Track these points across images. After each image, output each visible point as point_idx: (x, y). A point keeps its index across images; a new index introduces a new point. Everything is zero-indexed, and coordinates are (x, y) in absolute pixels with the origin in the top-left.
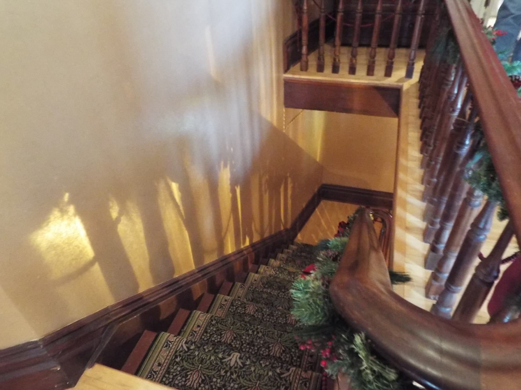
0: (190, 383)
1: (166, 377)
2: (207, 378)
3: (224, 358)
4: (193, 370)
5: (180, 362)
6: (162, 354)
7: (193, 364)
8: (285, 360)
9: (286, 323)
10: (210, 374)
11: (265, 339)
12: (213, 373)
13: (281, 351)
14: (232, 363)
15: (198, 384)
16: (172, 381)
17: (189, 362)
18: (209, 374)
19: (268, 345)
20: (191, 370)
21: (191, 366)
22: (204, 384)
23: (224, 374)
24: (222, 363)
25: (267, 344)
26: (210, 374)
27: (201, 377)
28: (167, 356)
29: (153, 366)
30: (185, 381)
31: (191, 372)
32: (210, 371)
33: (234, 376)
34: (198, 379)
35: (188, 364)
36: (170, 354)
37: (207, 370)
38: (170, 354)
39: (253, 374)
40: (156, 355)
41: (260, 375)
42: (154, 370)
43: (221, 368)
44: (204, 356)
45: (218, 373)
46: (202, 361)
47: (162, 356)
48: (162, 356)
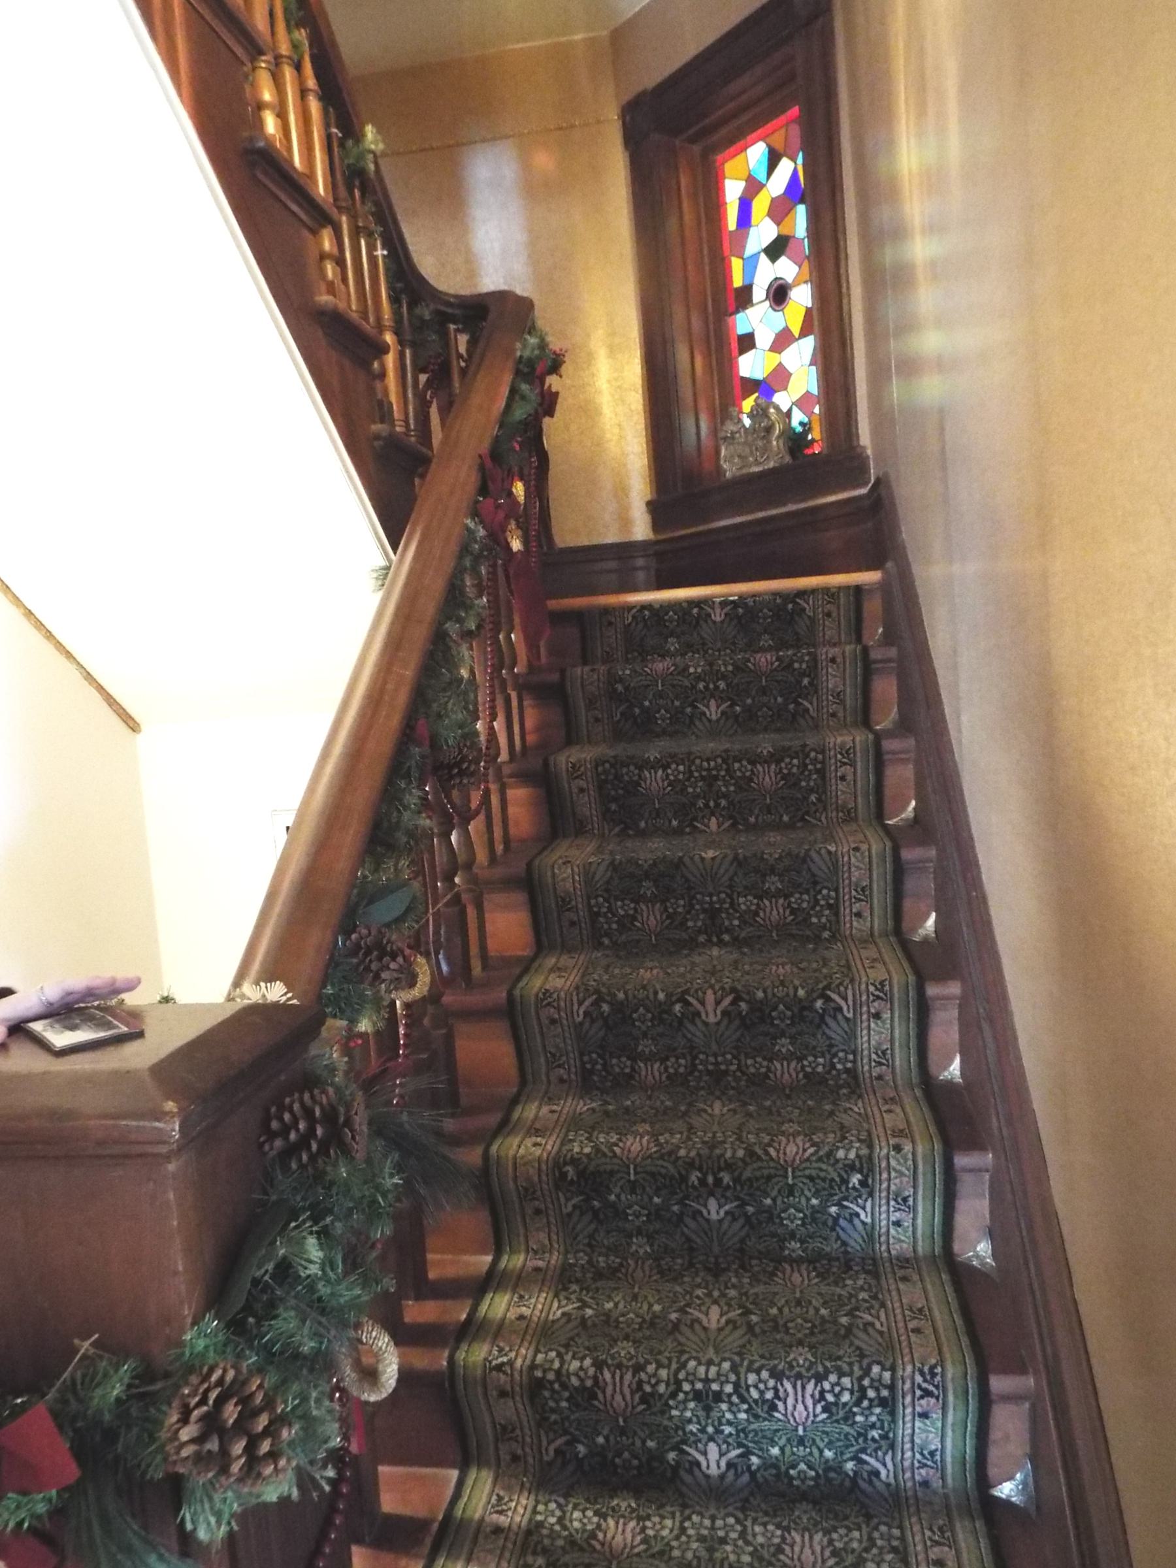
0: (779, 905)
1: (886, 1387)
2: (751, 921)
3: (731, 706)
4: (772, 671)
5: (849, 1176)
6: (905, 1179)
7: (811, 1178)
8: (583, 1511)
9: (663, 902)
10: (755, 1166)
11: (674, 1163)
12: (749, 1169)
13: (639, 917)
14: (713, 703)
15: (781, 1394)
16: (815, 896)
17: (824, 1180)
18: (760, 1164)
19: (649, 1407)
20: (808, 1160)
21: (814, 1173)
22: (765, 1401)
23: (722, 1174)
24: (730, 699)
25: (678, 789)
26: (755, 1166)
27: (778, 1151)
28: (889, 1180)
29: (855, 773)
30: (822, 1392)
31: (807, 1154)
32: (758, 1174)
33: (701, 685)
34: (790, 1408)
35: (822, 1174)
36: (885, 1185)
37: (766, 1172)
38: (885, 1185)
39: (669, 815)
40: (848, 671)
41: (658, 816)
42: (933, 1401)
43: (735, 1188)
44: (765, 699)
45: (736, 1174)
46: (764, 691)
47: (835, 676)
48: (858, 868)
